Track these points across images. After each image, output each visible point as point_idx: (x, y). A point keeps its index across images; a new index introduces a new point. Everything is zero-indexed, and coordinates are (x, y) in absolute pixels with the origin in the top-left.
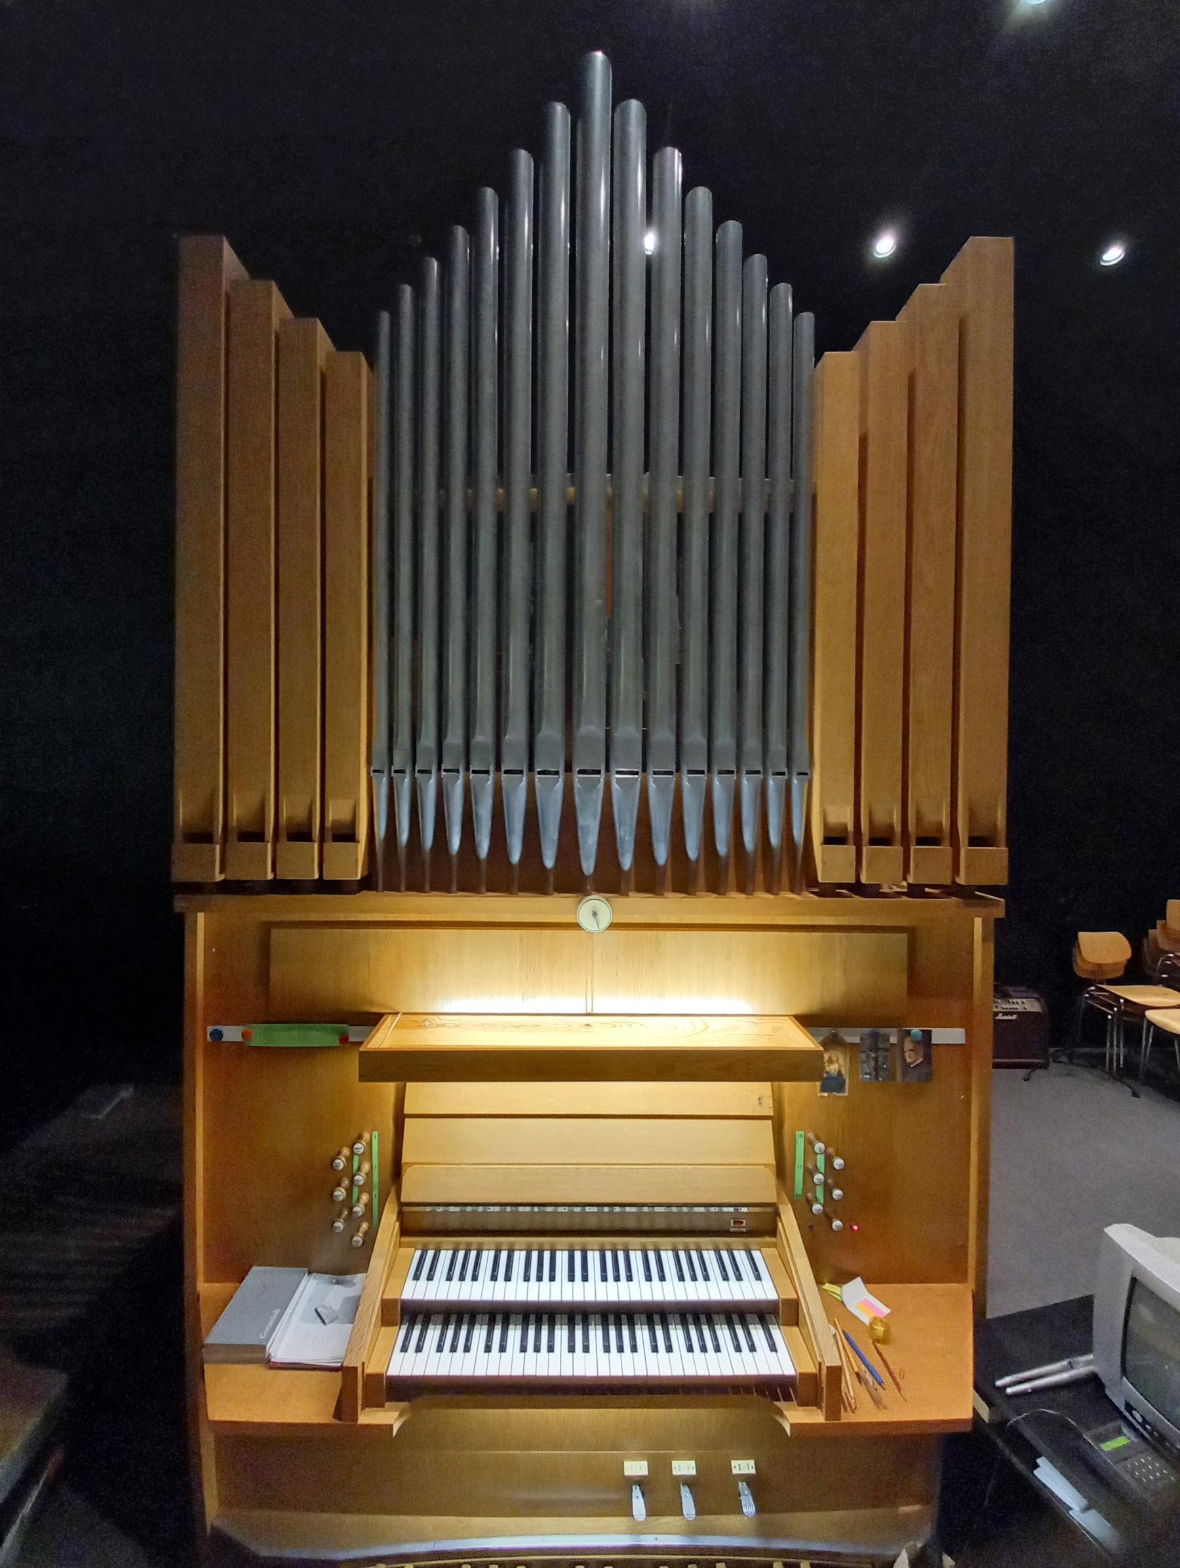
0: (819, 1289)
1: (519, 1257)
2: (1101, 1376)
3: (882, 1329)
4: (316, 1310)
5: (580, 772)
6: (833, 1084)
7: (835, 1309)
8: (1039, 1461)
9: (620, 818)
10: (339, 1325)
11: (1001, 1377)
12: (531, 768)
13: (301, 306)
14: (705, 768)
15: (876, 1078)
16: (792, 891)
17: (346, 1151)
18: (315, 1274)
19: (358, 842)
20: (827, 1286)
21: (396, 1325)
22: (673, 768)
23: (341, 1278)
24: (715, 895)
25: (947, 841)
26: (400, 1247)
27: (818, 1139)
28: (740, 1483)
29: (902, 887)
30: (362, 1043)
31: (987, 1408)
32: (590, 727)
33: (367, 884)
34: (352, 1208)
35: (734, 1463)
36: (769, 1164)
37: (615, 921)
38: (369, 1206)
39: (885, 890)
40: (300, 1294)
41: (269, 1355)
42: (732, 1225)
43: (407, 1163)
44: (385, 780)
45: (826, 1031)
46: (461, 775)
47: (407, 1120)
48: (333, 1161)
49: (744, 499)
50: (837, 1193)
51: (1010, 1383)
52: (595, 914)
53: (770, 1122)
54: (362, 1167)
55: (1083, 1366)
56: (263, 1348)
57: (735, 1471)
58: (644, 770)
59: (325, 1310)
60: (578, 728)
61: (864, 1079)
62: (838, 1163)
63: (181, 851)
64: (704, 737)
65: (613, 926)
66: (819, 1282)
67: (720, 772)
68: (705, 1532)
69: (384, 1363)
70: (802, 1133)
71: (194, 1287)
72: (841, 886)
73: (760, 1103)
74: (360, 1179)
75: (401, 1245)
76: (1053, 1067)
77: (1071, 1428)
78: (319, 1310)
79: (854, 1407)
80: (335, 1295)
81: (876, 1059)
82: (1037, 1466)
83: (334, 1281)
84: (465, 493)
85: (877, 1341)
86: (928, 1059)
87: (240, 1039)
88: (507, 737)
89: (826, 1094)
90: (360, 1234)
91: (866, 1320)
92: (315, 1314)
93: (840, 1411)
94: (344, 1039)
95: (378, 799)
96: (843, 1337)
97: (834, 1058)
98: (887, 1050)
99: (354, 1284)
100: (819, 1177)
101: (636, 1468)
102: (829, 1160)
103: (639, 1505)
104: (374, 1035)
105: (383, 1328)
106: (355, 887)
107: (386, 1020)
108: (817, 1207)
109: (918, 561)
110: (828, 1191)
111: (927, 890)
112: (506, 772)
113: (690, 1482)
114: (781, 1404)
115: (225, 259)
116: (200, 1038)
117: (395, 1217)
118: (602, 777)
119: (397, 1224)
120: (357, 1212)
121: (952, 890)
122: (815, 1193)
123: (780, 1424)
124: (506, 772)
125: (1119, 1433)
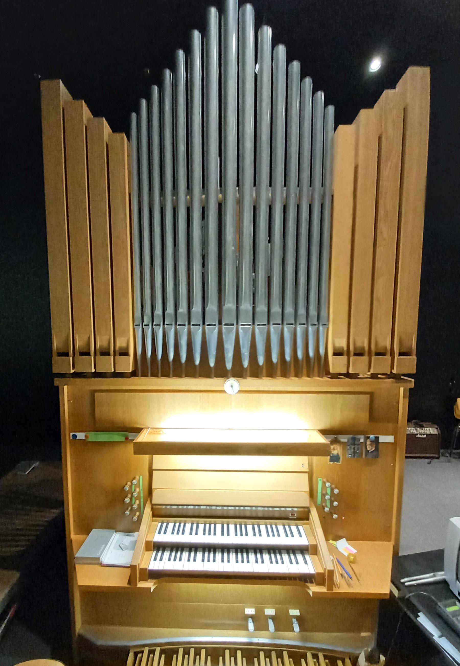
0: (326, 543)
1: (201, 526)
2: (447, 580)
3: (353, 558)
4: (119, 545)
5: (226, 325)
6: (335, 459)
7: (333, 550)
8: (419, 614)
9: (243, 344)
10: (129, 551)
11: (403, 578)
12: (204, 323)
13: (96, 113)
14: (280, 322)
15: (354, 456)
16: (319, 376)
17: (129, 483)
18: (118, 532)
19: (130, 356)
20: (331, 541)
21: (151, 551)
22: (266, 323)
23: (129, 534)
24: (285, 378)
25: (366, 354)
26: (152, 522)
27: (328, 481)
28: (293, 619)
29: (368, 375)
30: (134, 440)
31: (397, 591)
32: (230, 305)
33: (134, 374)
34: (132, 506)
35: (290, 611)
36: (306, 491)
37: (241, 389)
38: (139, 505)
39: (361, 376)
40: (113, 538)
41: (101, 562)
42: (290, 515)
43: (154, 488)
44: (140, 329)
45: (333, 437)
46: (173, 326)
47: (154, 471)
48: (124, 487)
49: (300, 198)
50: (335, 504)
51: (407, 581)
52: (232, 386)
53: (307, 474)
54: (136, 489)
55: (439, 576)
56: (98, 559)
57: (291, 614)
58: (254, 323)
59: (122, 545)
60: (224, 305)
61: (348, 457)
62: (336, 491)
63: (56, 359)
64: (280, 308)
65: (240, 392)
66: (327, 539)
67: (287, 324)
68: (279, 638)
69: (147, 565)
70: (321, 479)
71: (70, 537)
72: (341, 374)
73: (303, 466)
74: (135, 494)
75: (153, 521)
76: (442, 458)
77: (433, 601)
78: (121, 545)
79: (339, 586)
80: (127, 540)
81: (354, 449)
82: (418, 616)
83: (126, 535)
84: (173, 199)
85: (350, 562)
86: (377, 449)
87: (84, 438)
88: (193, 309)
89: (332, 463)
90: (136, 516)
91: (346, 554)
92: (119, 546)
93: (333, 588)
94: (127, 438)
95: (138, 338)
96: (336, 561)
97: (336, 448)
98: (359, 445)
99: (134, 536)
100: (327, 497)
101: (250, 611)
102: (332, 490)
103: (251, 626)
104: (139, 437)
105: (146, 552)
106: (129, 375)
107: (144, 430)
108: (327, 509)
109: (381, 225)
110: (332, 503)
111: (379, 376)
112: (193, 325)
113: (273, 618)
114: (308, 584)
115: (61, 90)
116: (67, 438)
117: (150, 509)
118: (235, 327)
119: (151, 512)
120: (134, 508)
121: (391, 376)
122: (326, 503)
123: (308, 592)
124: (193, 325)
125: (455, 604)
